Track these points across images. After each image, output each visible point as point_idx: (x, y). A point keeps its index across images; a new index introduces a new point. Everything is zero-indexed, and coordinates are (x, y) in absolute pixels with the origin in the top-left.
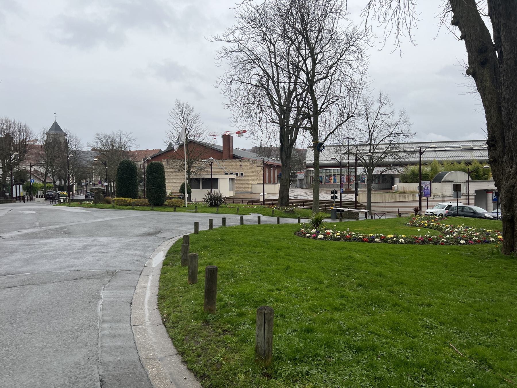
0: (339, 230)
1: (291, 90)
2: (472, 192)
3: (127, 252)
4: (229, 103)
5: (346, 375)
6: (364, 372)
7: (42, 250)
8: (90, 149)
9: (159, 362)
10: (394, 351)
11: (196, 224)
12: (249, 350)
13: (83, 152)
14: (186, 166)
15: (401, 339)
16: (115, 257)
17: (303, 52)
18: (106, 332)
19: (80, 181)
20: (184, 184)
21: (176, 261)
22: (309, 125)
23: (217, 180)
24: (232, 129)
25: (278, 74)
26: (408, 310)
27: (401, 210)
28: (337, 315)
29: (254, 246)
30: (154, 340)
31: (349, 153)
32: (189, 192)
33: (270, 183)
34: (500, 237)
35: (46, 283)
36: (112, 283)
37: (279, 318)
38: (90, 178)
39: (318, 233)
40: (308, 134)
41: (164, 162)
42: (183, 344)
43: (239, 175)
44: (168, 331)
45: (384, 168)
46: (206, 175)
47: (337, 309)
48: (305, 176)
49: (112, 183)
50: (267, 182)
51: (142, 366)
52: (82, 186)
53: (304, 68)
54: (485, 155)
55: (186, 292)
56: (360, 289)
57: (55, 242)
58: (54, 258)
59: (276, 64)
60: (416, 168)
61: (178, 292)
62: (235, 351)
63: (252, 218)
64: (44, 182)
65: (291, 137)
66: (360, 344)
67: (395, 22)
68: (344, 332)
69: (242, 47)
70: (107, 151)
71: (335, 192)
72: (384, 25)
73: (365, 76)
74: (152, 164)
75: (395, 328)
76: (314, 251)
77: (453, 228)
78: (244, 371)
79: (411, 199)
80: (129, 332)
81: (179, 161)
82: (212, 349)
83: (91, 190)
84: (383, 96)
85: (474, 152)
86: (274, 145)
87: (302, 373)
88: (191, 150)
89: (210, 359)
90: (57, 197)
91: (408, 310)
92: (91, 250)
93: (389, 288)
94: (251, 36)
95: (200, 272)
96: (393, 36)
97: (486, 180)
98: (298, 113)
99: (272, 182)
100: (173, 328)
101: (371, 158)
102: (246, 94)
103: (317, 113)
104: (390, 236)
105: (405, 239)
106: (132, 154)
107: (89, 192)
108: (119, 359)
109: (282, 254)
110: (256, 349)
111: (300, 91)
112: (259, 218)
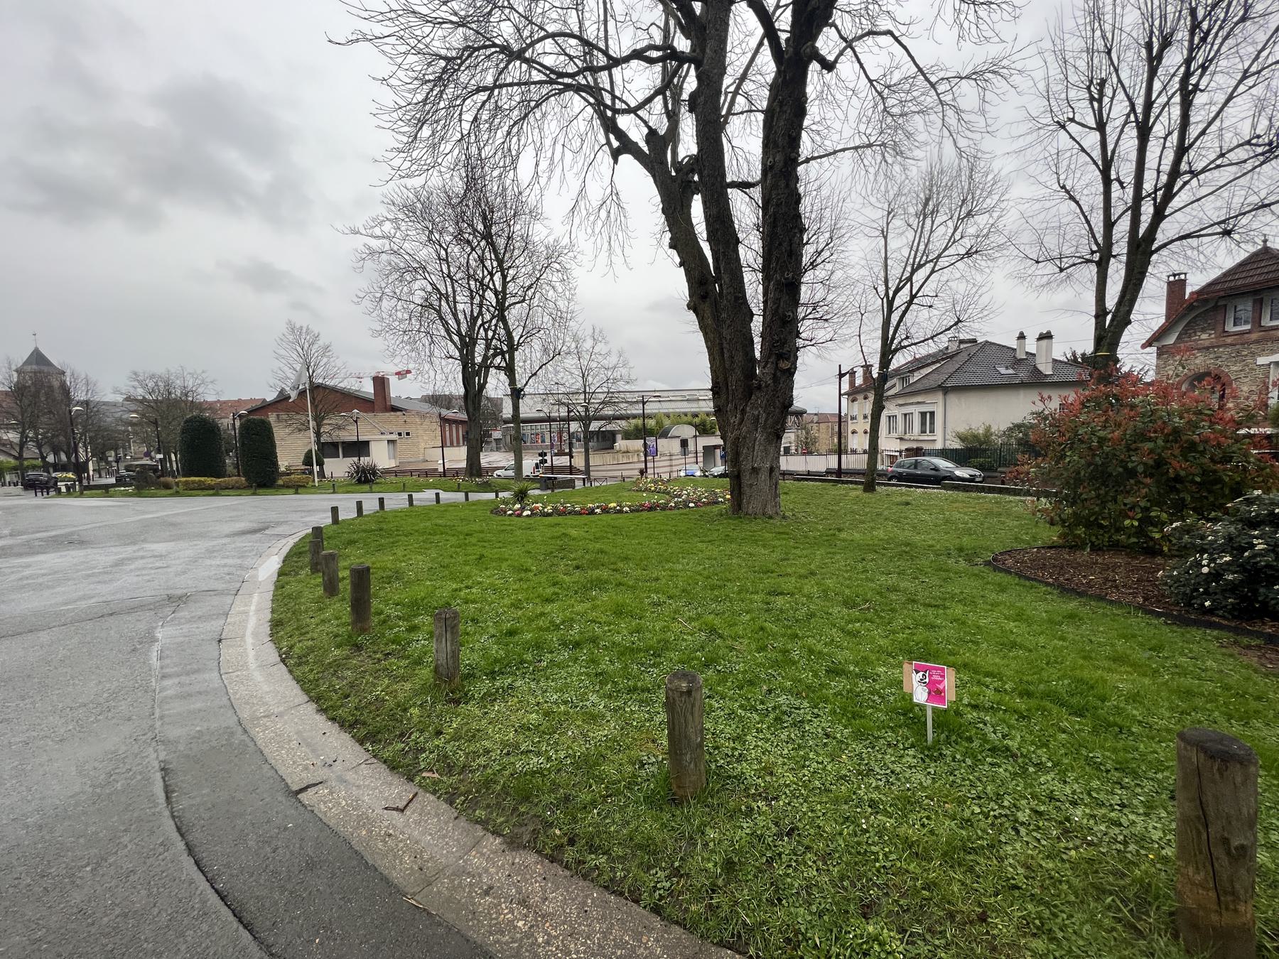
0: (550, 502)
1: (475, 315)
2: (700, 449)
3: (208, 562)
4: (379, 328)
5: (561, 678)
6: (583, 670)
7: (19, 575)
8: (120, 398)
9: (277, 719)
10: (618, 638)
11: (335, 510)
12: (425, 673)
13: (105, 404)
14: (312, 424)
15: (625, 623)
16: (184, 573)
17: (488, 263)
18: (170, 692)
19: (103, 453)
20: (309, 453)
21: (301, 568)
22: (503, 364)
23: (367, 443)
24: (388, 368)
25: (454, 292)
26: (633, 588)
27: (625, 473)
28: (548, 608)
29: (430, 534)
30: (266, 688)
31: (560, 403)
32: (320, 464)
33: (452, 445)
34: (728, 497)
35: (31, 631)
36: (177, 615)
37: (470, 623)
38: (124, 448)
39: (523, 509)
40: (503, 376)
41: (272, 418)
42: (318, 686)
43: (404, 435)
44: (291, 672)
45: (602, 422)
46: (348, 435)
47: (548, 601)
48: (504, 436)
49: (173, 455)
50: (448, 444)
51: (245, 731)
52: (108, 463)
53: (491, 286)
54: (709, 406)
55: (320, 609)
56: (577, 572)
57: (51, 560)
58: (53, 587)
59: (449, 276)
60: (640, 422)
61: (306, 611)
62: (404, 679)
63: (425, 497)
64: (20, 457)
65: (479, 380)
66: (577, 638)
67: (606, 239)
68: (557, 627)
69: (396, 248)
70: (156, 401)
71: (543, 454)
72: (593, 239)
73: (572, 303)
74: (249, 421)
75: (619, 612)
76: (518, 533)
77: (682, 490)
78: (419, 703)
79: (635, 459)
80: (217, 683)
81: (298, 417)
82: (367, 683)
83: (128, 468)
84: (597, 331)
85: (701, 402)
86: (455, 392)
87: (503, 688)
88: (319, 398)
89: (365, 698)
90: (51, 484)
91: (633, 588)
92: (132, 567)
93: (612, 566)
94: (409, 233)
95: (344, 578)
96: (604, 255)
97: (713, 434)
98: (488, 347)
99: (455, 444)
100: (300, 665)
101: (587, 409)
102: (406, 316)
103: (512, 348)
104: (612, 505)
105: (629, 507)
106: (211, 406)
107: (123, 472)
108: (198, 728)
109: (474, 540)
110: (436, 670)
111: (488, 317)
112: (437, 495)
